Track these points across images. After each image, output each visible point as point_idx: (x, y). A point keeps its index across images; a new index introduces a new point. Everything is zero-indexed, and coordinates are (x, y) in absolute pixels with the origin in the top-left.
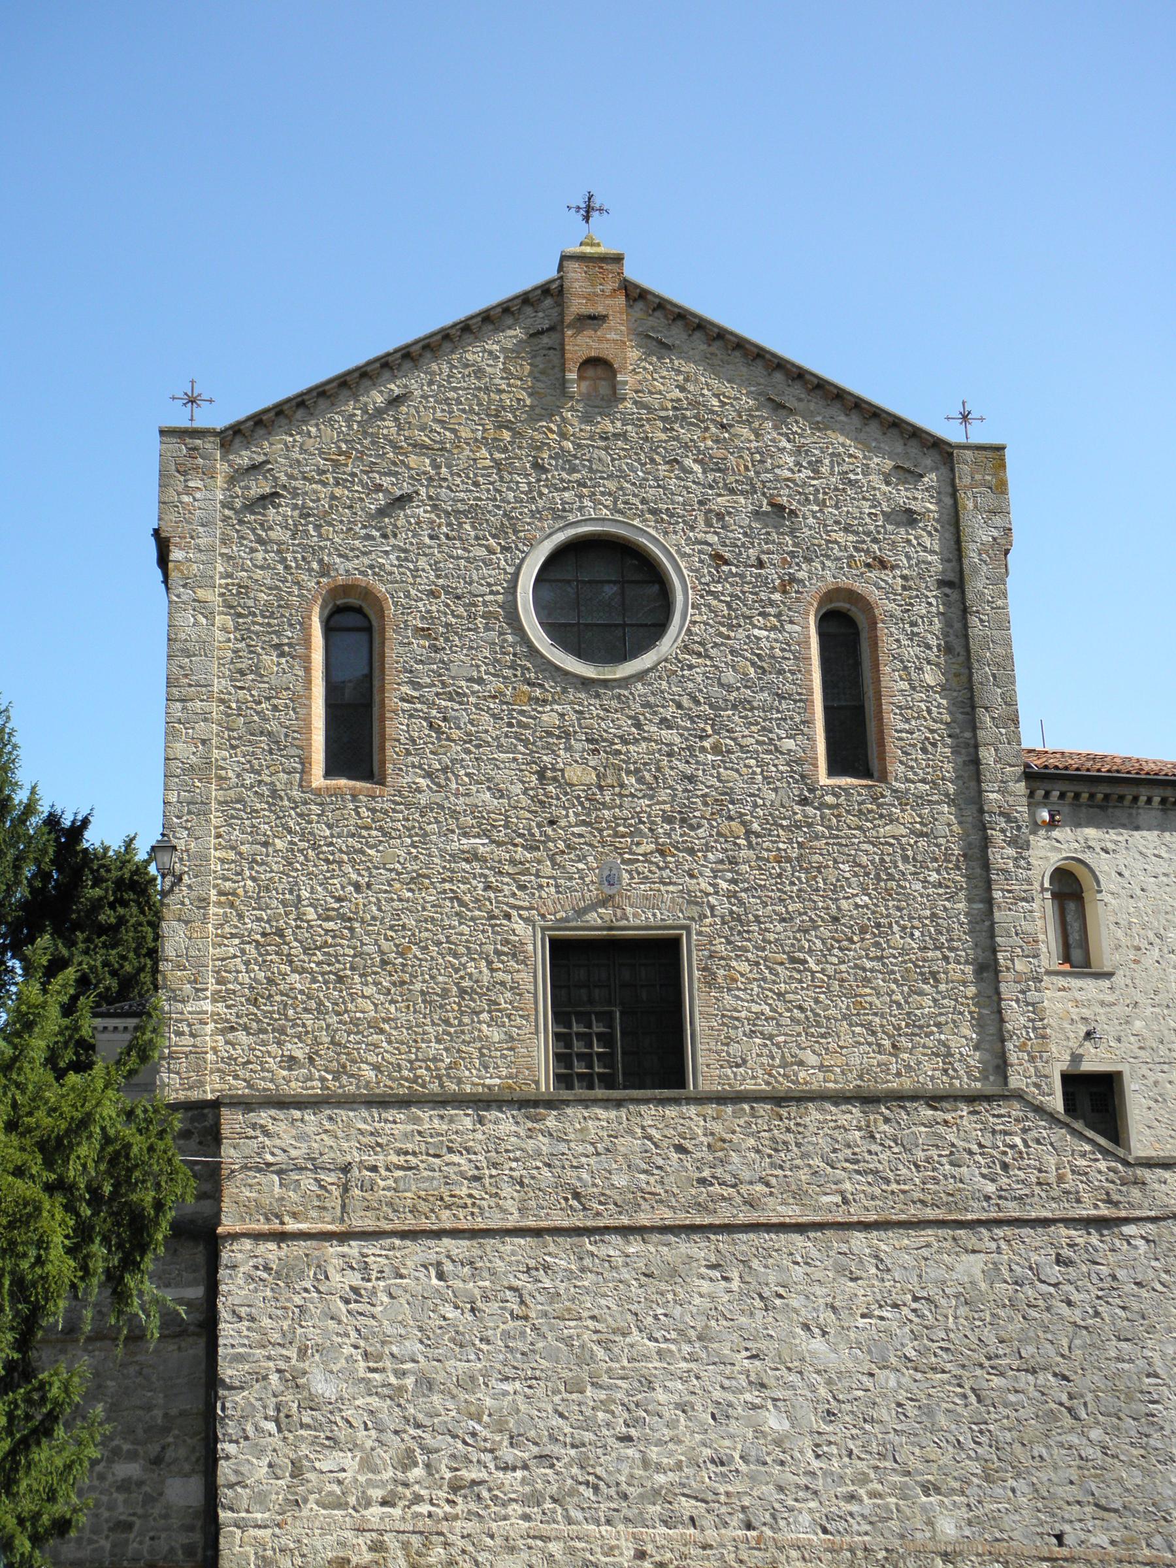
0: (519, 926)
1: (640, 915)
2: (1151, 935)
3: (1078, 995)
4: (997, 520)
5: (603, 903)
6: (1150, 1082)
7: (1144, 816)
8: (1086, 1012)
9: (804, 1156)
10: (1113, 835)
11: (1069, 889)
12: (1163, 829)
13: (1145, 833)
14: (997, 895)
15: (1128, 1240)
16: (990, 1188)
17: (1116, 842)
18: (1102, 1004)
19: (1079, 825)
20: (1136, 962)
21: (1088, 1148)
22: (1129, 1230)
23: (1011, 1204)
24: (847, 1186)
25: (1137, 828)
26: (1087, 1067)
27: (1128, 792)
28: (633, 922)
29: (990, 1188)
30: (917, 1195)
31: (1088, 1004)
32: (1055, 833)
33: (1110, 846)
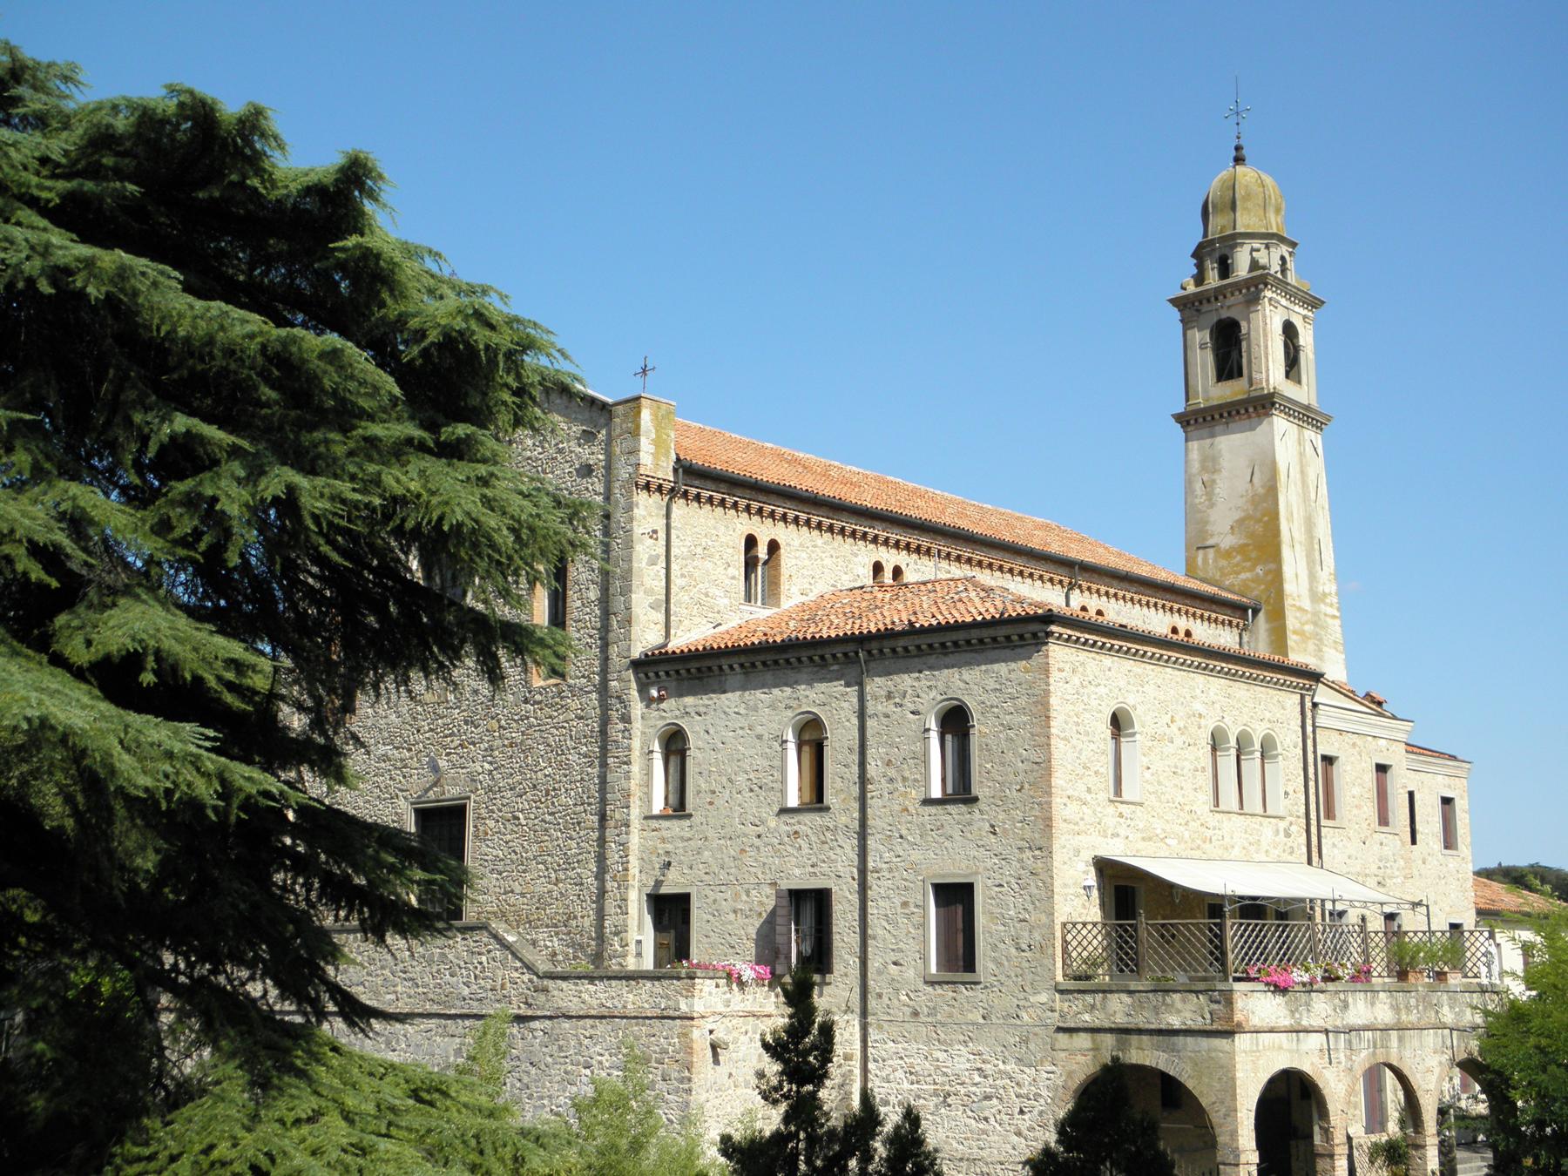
0: (402, 802)
1: (451, 792)
2: (724, 780)
3: (664, 833)
4: (633, 460)
5: (435, 784)
6: (709, 901)
7: (732, 680)
8: (669, 847)
9: (383, 968)
10: (705, 700)
11: (674, 744)
12: (744, 688)
13: (729, 695)
14: (610, 760)
15: (532, 1031)
16: (466, 992)
17: (707, 706)
18: (682, 839)
19: (681, 695)
20: (711, 803)
21: (519, 964)
22: (536, 1024)
23: (475, 1004)
24: (399, 988)
25: (724, 692)
26: (664, 890)
27: (713, 663)
28: (448, 796)
29: (466, 992)
30: (431, 996)
31: (670, 840)
32: (664, 705)
33: (702, 710)
